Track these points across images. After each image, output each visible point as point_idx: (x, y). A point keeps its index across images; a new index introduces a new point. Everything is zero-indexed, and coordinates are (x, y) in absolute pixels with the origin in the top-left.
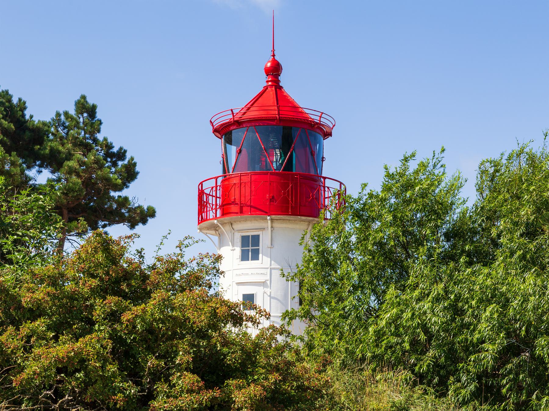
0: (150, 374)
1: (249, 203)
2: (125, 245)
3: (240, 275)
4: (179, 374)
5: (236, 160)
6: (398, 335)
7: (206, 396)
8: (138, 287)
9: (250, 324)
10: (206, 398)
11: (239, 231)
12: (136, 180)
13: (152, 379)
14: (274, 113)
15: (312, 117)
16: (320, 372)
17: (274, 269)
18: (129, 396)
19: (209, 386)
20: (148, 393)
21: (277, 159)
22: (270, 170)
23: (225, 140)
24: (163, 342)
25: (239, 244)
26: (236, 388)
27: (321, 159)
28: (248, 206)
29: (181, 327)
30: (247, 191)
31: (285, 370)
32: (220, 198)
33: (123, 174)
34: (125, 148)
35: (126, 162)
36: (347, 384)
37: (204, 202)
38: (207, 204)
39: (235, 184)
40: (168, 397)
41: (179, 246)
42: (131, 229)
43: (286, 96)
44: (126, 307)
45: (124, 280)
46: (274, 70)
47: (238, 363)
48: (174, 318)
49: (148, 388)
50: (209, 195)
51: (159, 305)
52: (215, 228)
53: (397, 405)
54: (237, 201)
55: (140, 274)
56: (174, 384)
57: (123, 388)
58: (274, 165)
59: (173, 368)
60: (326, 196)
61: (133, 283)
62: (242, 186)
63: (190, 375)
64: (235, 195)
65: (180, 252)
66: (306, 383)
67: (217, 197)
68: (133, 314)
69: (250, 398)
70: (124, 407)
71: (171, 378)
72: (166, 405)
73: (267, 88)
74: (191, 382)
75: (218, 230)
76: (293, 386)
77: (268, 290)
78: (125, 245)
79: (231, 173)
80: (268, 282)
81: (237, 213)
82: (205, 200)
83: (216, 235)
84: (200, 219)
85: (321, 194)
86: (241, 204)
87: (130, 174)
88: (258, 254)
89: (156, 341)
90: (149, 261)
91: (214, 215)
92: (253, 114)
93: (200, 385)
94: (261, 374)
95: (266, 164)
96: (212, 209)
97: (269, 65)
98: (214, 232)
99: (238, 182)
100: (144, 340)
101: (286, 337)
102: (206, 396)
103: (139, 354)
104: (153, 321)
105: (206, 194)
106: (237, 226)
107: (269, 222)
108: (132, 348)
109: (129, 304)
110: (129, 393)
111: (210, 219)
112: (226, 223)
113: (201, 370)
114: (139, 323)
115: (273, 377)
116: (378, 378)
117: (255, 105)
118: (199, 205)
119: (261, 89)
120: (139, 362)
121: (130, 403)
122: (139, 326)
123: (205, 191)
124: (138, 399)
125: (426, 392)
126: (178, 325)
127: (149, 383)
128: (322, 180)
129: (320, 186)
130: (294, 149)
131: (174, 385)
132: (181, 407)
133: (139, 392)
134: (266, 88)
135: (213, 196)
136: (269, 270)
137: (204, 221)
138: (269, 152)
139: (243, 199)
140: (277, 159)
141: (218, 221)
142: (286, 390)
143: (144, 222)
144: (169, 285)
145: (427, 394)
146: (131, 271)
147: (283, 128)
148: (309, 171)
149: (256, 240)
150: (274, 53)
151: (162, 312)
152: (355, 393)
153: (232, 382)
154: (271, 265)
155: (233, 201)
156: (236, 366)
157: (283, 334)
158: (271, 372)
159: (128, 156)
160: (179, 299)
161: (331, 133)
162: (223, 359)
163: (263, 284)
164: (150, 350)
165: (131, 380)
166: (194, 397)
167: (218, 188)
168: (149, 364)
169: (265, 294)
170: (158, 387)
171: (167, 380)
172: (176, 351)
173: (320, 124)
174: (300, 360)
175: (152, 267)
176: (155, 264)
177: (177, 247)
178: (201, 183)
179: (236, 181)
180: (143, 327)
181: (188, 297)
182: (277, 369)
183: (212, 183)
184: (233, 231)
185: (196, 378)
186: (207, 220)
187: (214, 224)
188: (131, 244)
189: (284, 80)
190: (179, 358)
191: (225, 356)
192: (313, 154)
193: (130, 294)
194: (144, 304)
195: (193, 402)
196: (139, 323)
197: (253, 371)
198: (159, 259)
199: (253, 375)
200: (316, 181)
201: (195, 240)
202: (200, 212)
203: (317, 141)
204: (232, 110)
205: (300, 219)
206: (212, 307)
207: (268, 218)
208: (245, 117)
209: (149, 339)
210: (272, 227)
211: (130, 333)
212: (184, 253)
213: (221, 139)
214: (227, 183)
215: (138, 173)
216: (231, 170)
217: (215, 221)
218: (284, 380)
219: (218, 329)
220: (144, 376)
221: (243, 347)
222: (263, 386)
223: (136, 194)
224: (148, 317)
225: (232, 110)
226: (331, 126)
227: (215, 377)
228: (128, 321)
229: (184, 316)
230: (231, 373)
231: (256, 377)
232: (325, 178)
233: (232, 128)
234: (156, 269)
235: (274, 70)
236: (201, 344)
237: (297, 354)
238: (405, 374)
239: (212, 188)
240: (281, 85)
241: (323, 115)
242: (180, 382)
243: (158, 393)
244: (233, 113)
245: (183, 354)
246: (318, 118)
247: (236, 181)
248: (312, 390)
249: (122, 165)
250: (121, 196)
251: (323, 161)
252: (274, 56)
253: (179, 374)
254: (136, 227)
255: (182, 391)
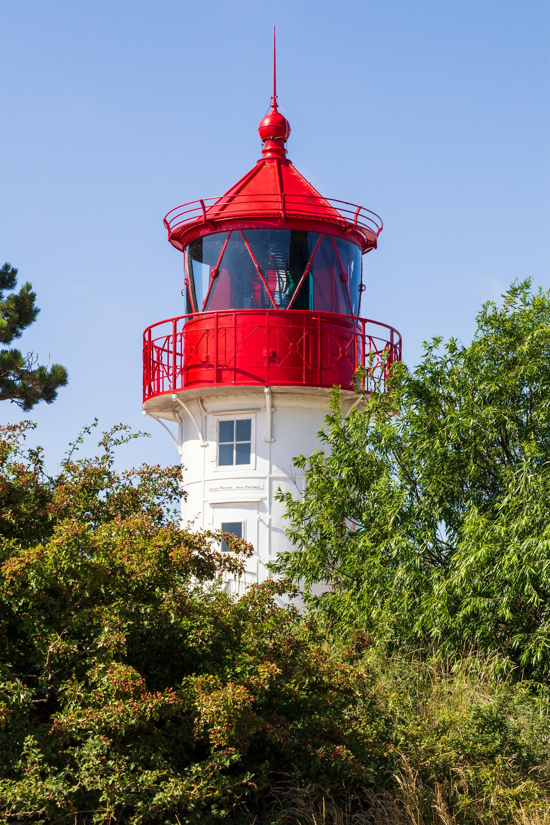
0: (52, 667)
1: (232, 364)
2: (10, 441)
3: (216, 490)
4: (102, 666)
5: (210, 289)
6: (487, 595)
7: (152, 702)
8: (33, 515)
9: (228, 576)
10: (150, 705)
11: (215, 413)
12: (34, 323)
13: (56, 675)
14: (276, 206)
15: (343, 214)
16: (351, 660)
17: (277, 479)
18: (15, 705)
19: (154, 684)
20: (49, 698)
21: (282, 285)
22: (269, 307)
23: (190, 253)
24: (76, 610)
25: (216, 435)
26: (203, 689)
27: (358, 288)
28: (231, 370)
29: (106, 584)
30: (228, 343)
31: (290, 657)
32: (181, 355)
33: (11, 314)
34: (14, 266)
35: (16, 291)
36: (400, 679)
37: (154, 362)
38: (158, 366)
39: (207, 331)
40: (84, 706)
41: (103, 443)
42: (25, 409)
43: (296, 177)
44: (10, 550)
45: (8, 504)
46: (277, 132)
47: (207, 646)
48: (94, 569)
49: (50, 691)
50: (163, 350)
51: (68, 545)
52: (173, 407)
53: (485, 715)
54: (212, 361)
55: (36, 493)
56: (94, 684)
57: (6, 692)
58: (277, 298)
59: (92, 655)
60: (366, 353)
61: (23, 507)
62: (221, 335)
63: (122, 668)
64: (207, 349)
65: (105, 453)
66: (325, 679)
67: (175, 354)
68: (21, 562)
69: (226, 708)
70: (7, 725)
71: (88, 673)
72: (80, 720)
73: (264, 164)
74: (122, 679)
75: (178, 412)
76: (304, 684)
77: (266, 517)
78: (10, 441)
79: (201, 312)
80: (267, 502)
81: (211, 382)
82: (155, 359)
83: (175, 420)
84: (147, 392)
85: (358, 348)
86: (218, 365)
87: (24, 311)
88: (249, 452)
89: (63, 608)
90: (52, 469)
91: (172, 384)
92: (239, 208)
93: (138, 683)
94: (248, 664)
95: (263, 296)
96: (168, 374)
97: (267, 122)
98: (170, 415)
99: (213, 327)
100: (42, 607)
101: (291, 597)
102: (152, 702)
103: (34, 631)
104: (57, 573)
105: (156, 347)
106: (212, 405)
107: (268, 397)
108: (21, 621)
109: (14, 544)
110: (16, 700)
111: (164, 393)
112: (192, 400)
113: (143, 658)
114: (33, 578)
115: (267, 671)
116: (454, 668)
117: (243, 192)
118: (144, 368)
119: (253, 165)
120: (33, 646)
121: (18, 717)
122: (33, 583)
123: (156, 343)
124: (32, 711)
125: (534, 691)
126: (102, 580)
127: (51, 682)
128: (360, 324)
129: (356, 335)
130: (310, 270)
131: (94, 686)
132: (108, 723)
133: (33, 697)
134: (261, 164)
135: (168, 352)
136: (268, 479)
137: (155, 395)
138: (266, 273)
139: (221, 357)
140: (282, 285)
141: (178, 396)
142: (291, 691)
143: (50, 396)
144: (87, 509)
145: (537, 695)
146: (21, 488)
147: (292, 233)
148: (337, 308)
149: (244, 428)
150: (275, 103)
151: (73, 557)
152: (412, 695)
153: (195, 679)
154: (270, 473)
155: (204, 360)
156: (204, 652)
157: (284, 592)
158: (262, 661)
159: (20, 282)
160: (101, 534)
161: (376, 242)
162: (181, 640)
163: (258, 505)
164: (54, 624)
165: (20, 678)
166: (129, 706)
167: (179, 337)
168: (51, 649)
169: (260, 523)
170: (66, 689)
171: (82, 676)
172: (99, 625)
173: (356, 227)
174: (318, 639)
175: (57, 481)
176: (62, 476)
177: (100, 444)
178: (149, 330)
179: (209, 325)
180: (40, 584)
181: (119, 530)
182: (274, 655)
183: (168, 329)
184: (205, 414)
185: (132, 671)
186: (158, 393)
187: (171, 401)
188: (20, 439)
189: (293, 149)
190: (103, 638)
191: (185, 633)
192: (343, 278)
193: (19, 527)
194: (40, 545)
195: (128, 715)
196: (33, 578)
197: (234, 659)
198: (68, 466)
199: (233, 667)
200: (349, 326)
201: (134, 432)
202: (147, 380)
203: (350, 257)
204: (202, 201)
205: (321, 391)
206: (160, 547)
207: (266, 390)
208: (225, 213)
209: (51, 605)
210: (272, 406)
211: (17, 595)
212: (112, 455)
213: (183, 251)
214: (193, 329)
215: (37, 311)
216: (201, 306)
217: (174, 396)
218: (287, 674)
219: (172, 586)
220: (42, 669)
221: (216, 618)
222: (248, 686)
223: (35, 347)
224: (49, 566)
225: (202, 201)
226: (376, 231)
227: (167, 671)
228: (14, 574)
229: (112, 564)
230: (195, 664)
231: (238, 670)
232: (364, 321)
233: (202, 233)
234: (63, 484)
235: (277, 132)
236: (142, 611)
237: (311, 628)
238: (501, 662)
239: (168, 337)
240: (287, 158)
241: (362, 212)
242: (104, 679)
243: (65, 699)
244: (204, 207)
245: (109, 631)
246: (353, 216)
247: (209, 325)
248: (337, 690)
249: (9, 298)
250: (6, 351)
251: (361, 291)
252: (275, 106)
253: (102, 666)
254: (35, 406)
255: (108, 696)
